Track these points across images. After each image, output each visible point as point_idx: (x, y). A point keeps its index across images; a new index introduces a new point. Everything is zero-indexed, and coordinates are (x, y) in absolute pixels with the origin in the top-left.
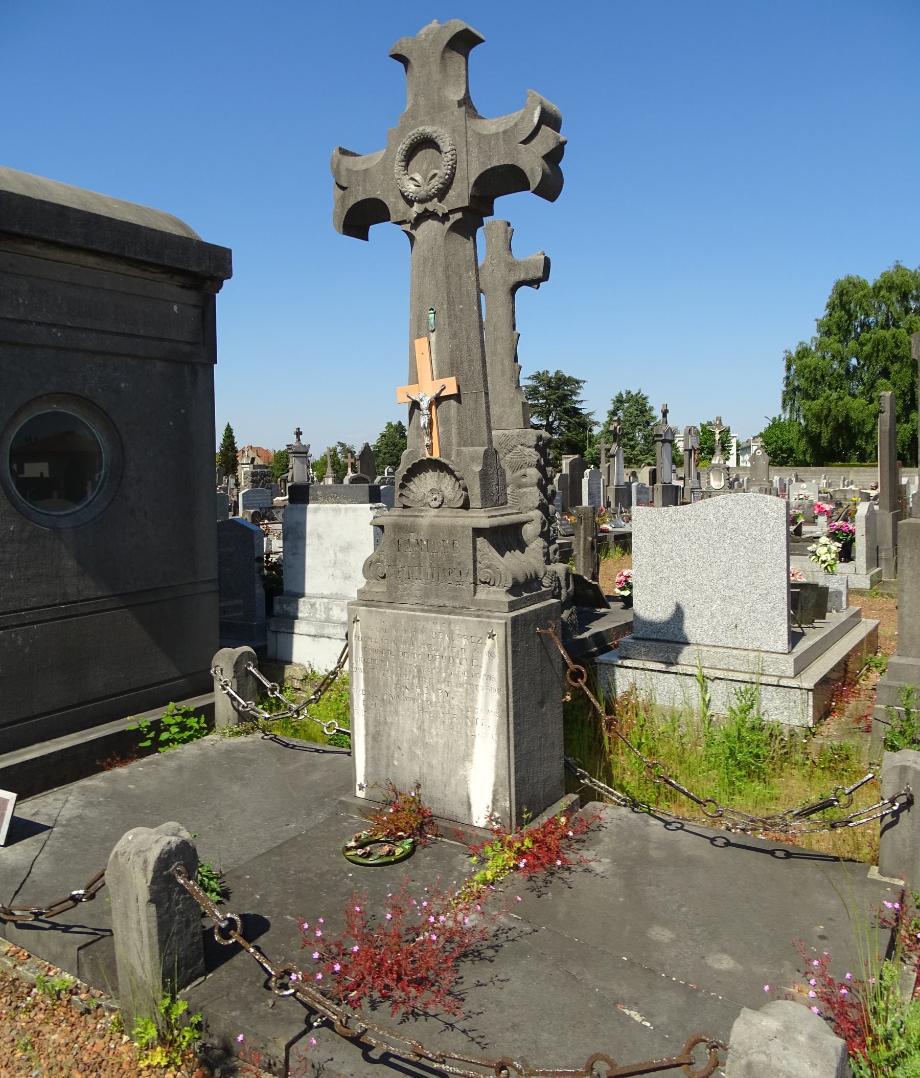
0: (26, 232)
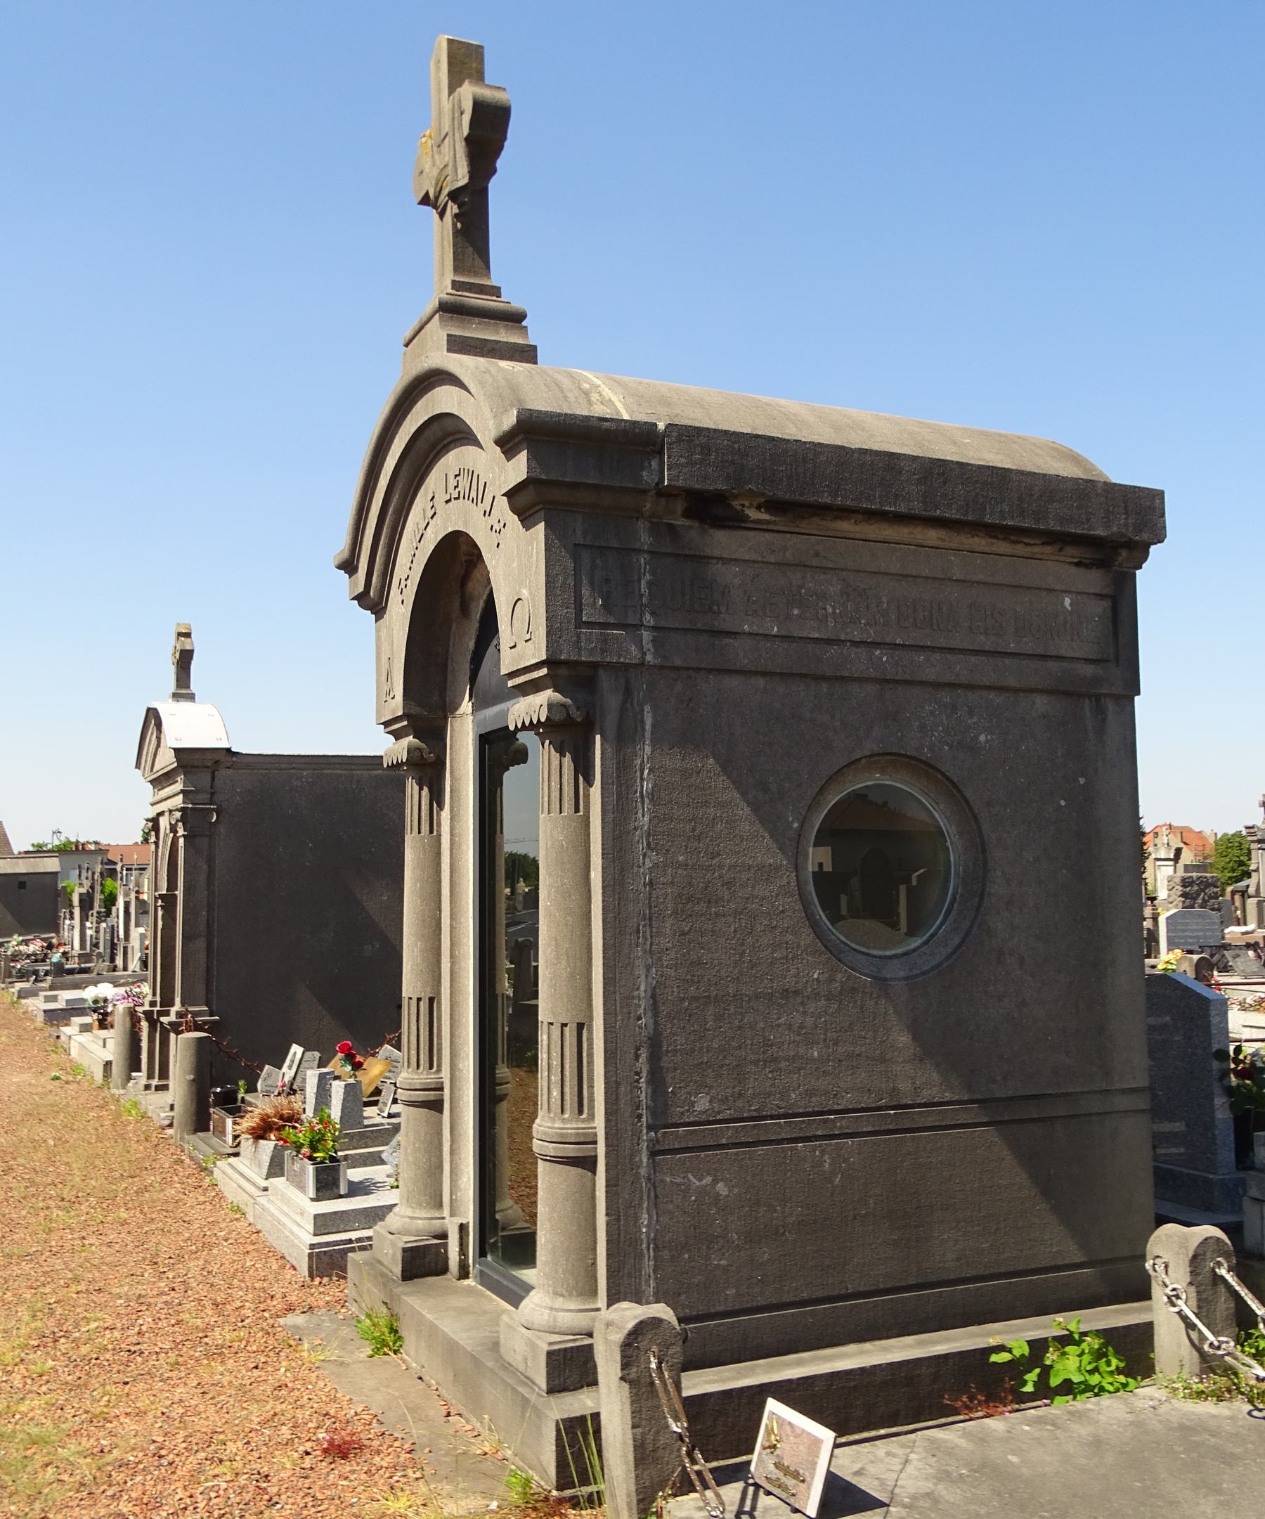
0: (839, 501)
